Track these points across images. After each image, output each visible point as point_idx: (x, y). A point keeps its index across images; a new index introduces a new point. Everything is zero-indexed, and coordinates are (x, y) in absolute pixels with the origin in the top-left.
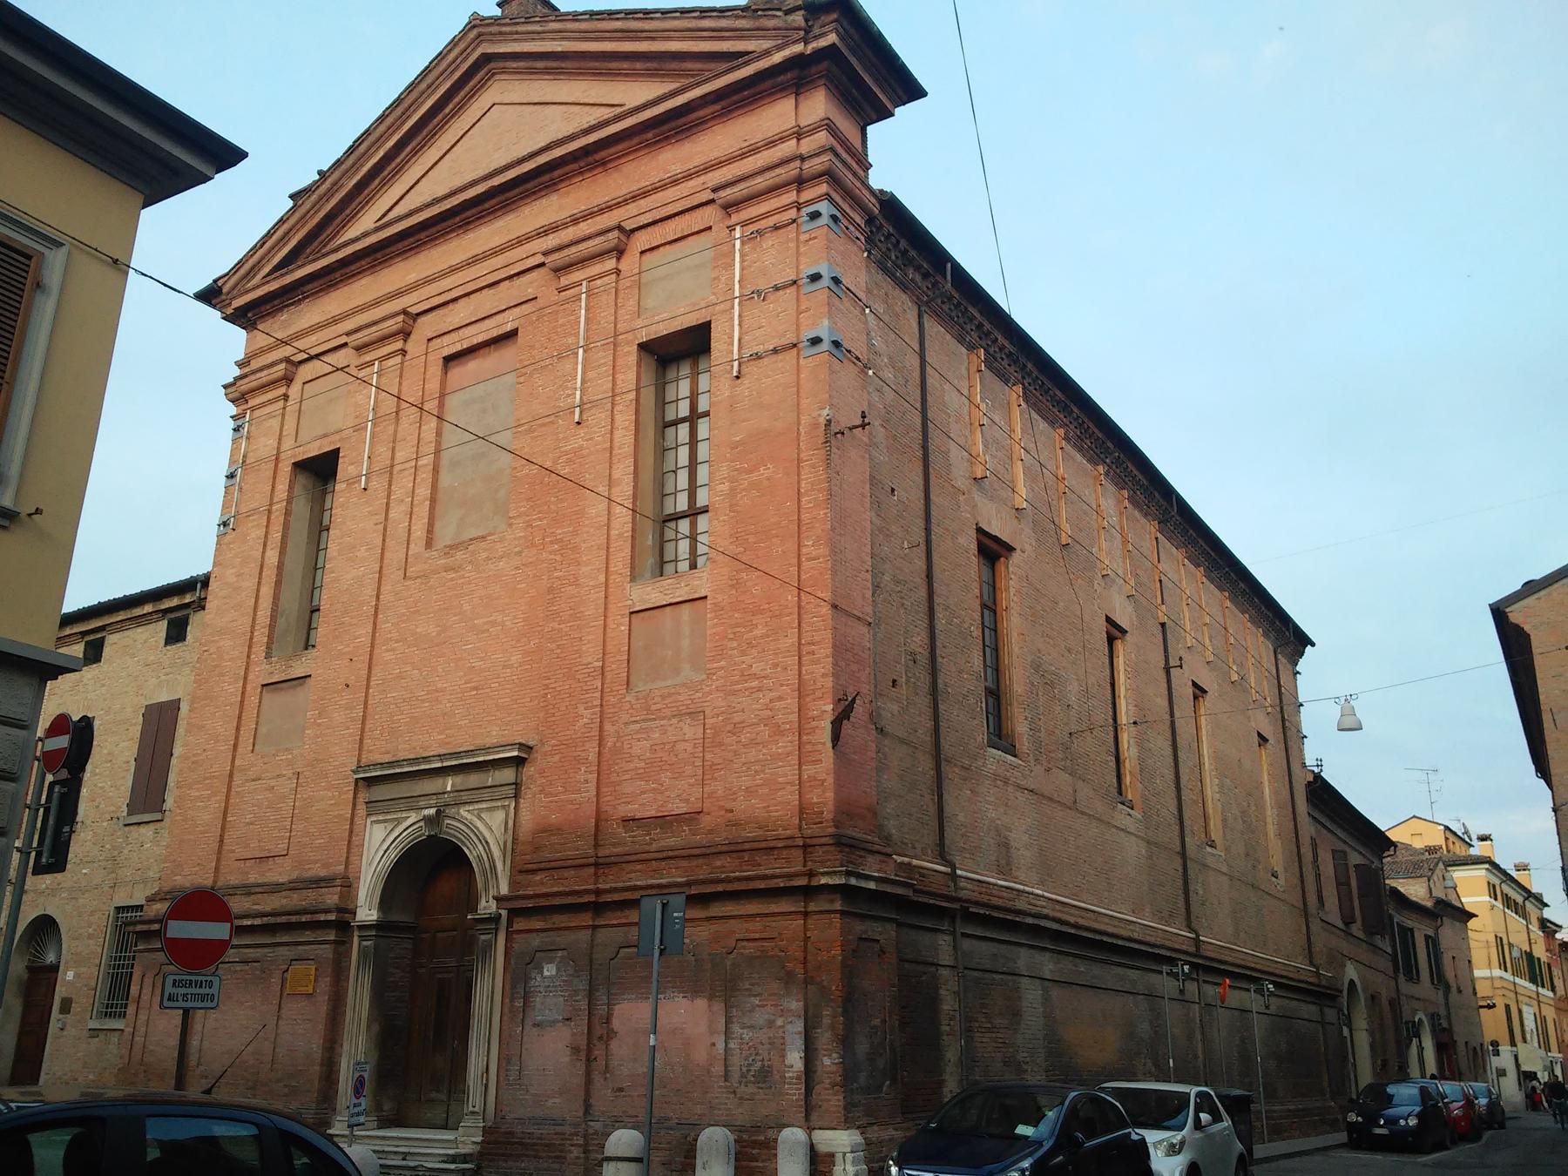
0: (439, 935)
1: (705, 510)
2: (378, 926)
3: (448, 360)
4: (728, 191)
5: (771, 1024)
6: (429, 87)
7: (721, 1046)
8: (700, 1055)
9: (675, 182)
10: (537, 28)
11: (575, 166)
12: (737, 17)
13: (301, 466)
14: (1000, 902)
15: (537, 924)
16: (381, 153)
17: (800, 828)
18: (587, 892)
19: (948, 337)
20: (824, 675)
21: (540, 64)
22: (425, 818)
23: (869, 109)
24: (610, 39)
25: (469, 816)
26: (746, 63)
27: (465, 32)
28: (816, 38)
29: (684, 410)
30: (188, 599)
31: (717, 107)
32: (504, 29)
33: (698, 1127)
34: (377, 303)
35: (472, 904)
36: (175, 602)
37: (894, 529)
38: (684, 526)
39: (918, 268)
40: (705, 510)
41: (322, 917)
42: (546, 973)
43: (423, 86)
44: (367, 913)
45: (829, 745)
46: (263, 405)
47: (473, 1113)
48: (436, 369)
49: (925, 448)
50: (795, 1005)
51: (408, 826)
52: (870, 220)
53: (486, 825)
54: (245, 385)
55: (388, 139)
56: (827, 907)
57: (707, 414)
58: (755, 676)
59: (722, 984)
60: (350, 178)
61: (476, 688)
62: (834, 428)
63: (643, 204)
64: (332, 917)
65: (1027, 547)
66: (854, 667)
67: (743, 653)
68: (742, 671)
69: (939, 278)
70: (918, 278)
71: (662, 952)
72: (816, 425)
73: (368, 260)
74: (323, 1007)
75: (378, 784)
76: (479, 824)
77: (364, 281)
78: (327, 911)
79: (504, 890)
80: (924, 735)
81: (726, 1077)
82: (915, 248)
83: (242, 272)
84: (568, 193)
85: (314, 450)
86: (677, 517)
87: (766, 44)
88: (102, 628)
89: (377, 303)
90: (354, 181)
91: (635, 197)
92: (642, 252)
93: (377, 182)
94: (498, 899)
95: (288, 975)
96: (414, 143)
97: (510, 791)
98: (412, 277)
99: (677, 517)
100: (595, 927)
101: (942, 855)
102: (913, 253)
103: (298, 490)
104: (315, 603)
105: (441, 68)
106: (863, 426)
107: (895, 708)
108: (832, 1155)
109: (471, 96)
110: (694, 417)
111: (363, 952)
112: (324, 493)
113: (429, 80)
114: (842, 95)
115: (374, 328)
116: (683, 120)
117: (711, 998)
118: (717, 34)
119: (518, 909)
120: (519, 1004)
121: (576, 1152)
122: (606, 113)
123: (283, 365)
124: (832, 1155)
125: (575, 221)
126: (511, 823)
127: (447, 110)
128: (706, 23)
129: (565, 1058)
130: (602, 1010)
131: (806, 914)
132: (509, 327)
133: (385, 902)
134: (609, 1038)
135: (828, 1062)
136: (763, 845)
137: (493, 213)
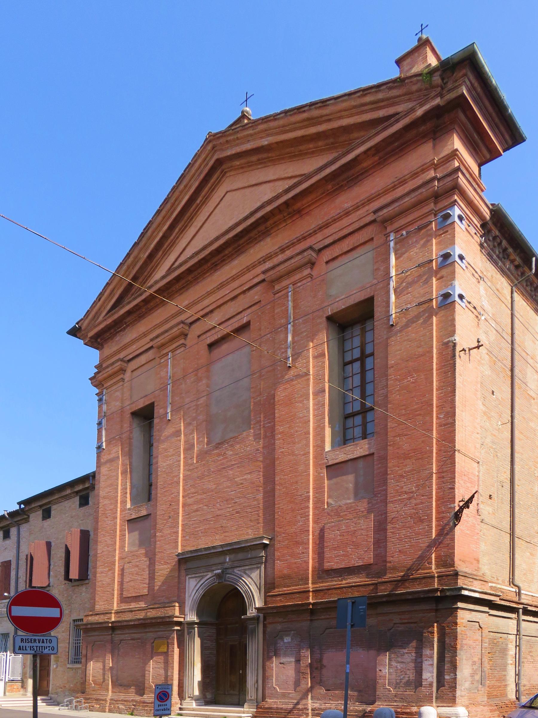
0: (229, 626)
3: (211, 346)
4: (385, 211)
6: (185, 186)
9: (347, 213)
10: (251, 132)
12: (390, 88)
13: (134, 414)
16: (161, 234)
19: (528, 308)
21: (254, 158)
22: (218, 576)
24: (301, 128)
25: (239, 573)
26: (397, 121)
27: (204, 147)
28: (449, 91)
29: (357, 354)
30: (87, 485)
34: (166, 321)
35: (244, 611)
36: (80, 487)
37: (493, 414)
38: (358, 420)
39: (512, 261)
42: (285, 641)
43: (182, 187)
46: (111, 386)
47: (251, 700)
48: (204, 350)
49: (512, 370)
52: (483, 226)
54: (100, 377)
55: (164, 224)
57: (372, 354)
58: (406, 493)
66: (469, 485)
67: (398, 481)
68: (397, 490)
69: (526, 269)
70: (512, 268)
71: (352, 626)
77: (159, 311)
82: (513, 247)
83: (90, 317)
85: (141, 404)
86: (353, 415)
87: (410, 105)
88: (49, 503)
89: (166, 321)
90: (147, 254)
91: (321, 228)
92: (327, 262)
93: (161, 253)
95: (154, 644)
96: (180, 226)
99: (353, 415)
101: (512, 582)
102: (510, 250)
103: (135, 425)
106: (478, 347)
107: (490, 510)
109: (213, 189)
110: (363, 358)
114: (466, 137)
115: (167, 334)
118: (376, 105)
123: (119, 363)
125: (283, 250)
127: (198, 201)
128: (368, 99)
131: (437, 610)
132: (245, 320)
134: (321, 668)
137: (231, 257)
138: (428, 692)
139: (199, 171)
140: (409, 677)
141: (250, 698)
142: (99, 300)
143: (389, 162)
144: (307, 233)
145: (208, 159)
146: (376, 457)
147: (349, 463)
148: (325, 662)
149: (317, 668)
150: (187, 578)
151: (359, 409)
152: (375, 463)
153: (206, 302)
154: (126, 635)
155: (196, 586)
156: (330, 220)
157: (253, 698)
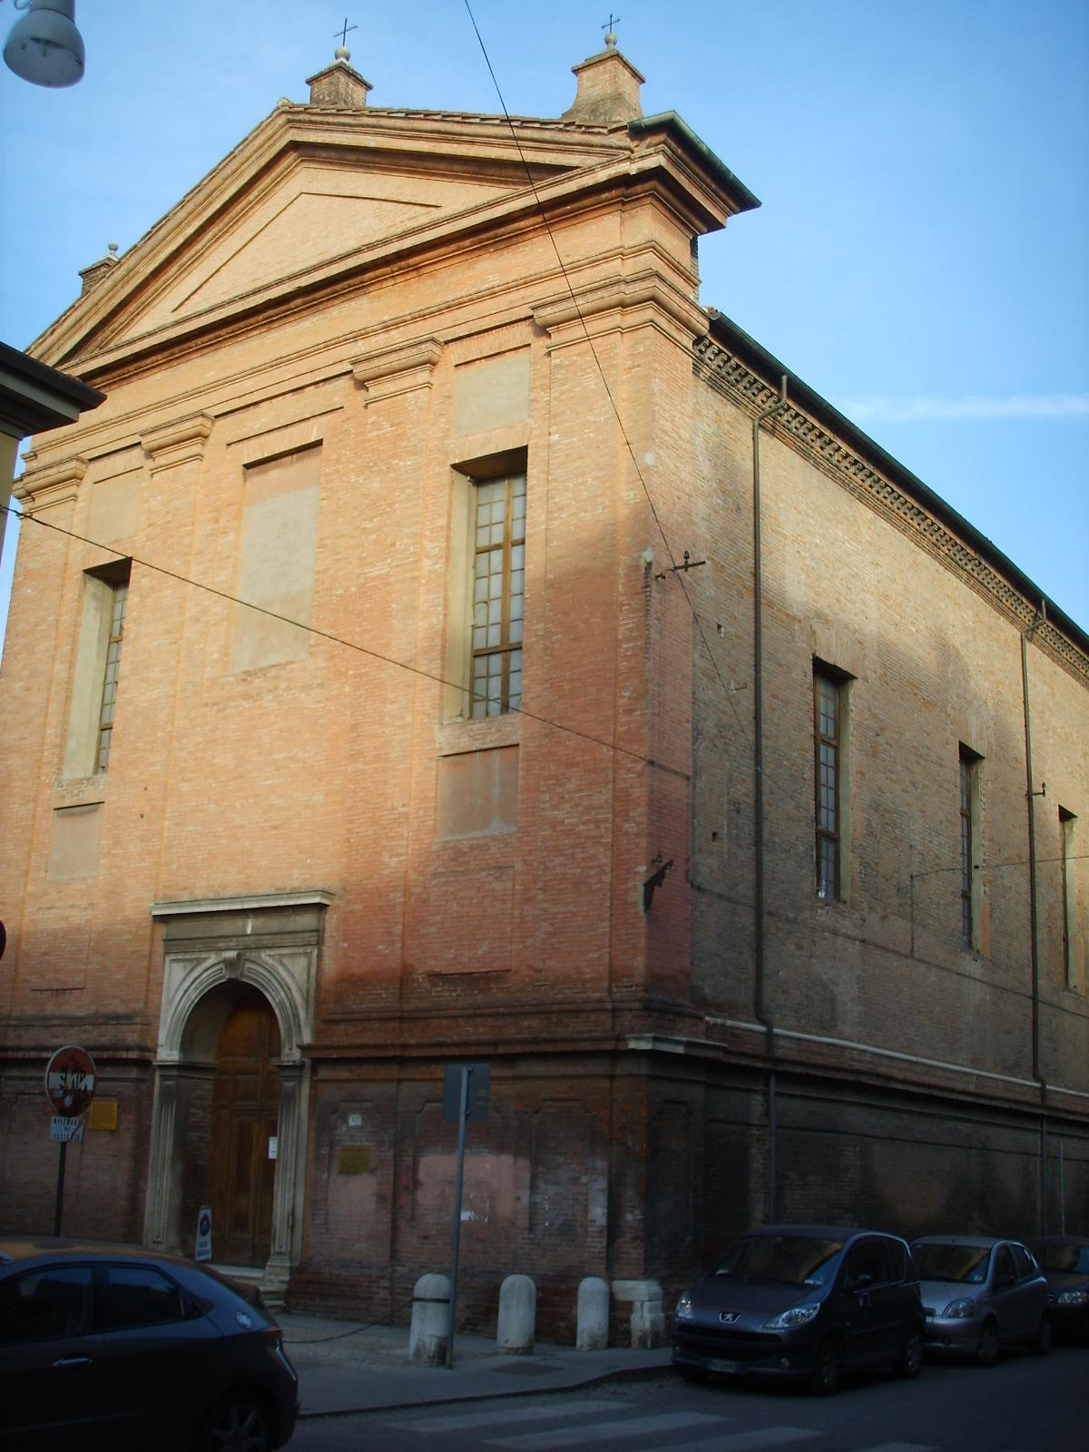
0: (239, 1077)
1: (518, 647)
2: (183, 1067)
5: (575, 1181)
7: (525, 1201)
8: (505, 1207)
9: (492, 294)
11: (388, 269)
14: (821, 1061)
15: (343, 1073)
17: (610, 991)
18: (393, 1046)
20: (637, 835)
22: (229, 964)
23: (698, 223)
25: (270, 961)
31: (539, 219)
32: (314, 118)
33: (501, 1276)
38: (496, 663)
40: (518, 647)
41: (124, 1055)
42: (352, 1123)
43: (228, 171)
44: (168, 1053)
45: (641, 907)
47: (279, 1253)
50: (601, 1164)
51: (208, 969)
52: (699, 339)
53: (288, 970)
55: (189, 224)
56: (635, 1070)
59: (527, 1141)
60: (147, 264)
61: (276, 828)
62: (655, 571)
63: (461, 315)
64: (133, 1055)
65: (870, 674)
67: (556, 807)
72: (636, 568)
73: (165, 354)
74: (128, 1142)
75: (180, 928)
76: (281, 969)
78: (128, 1049)
79: (307, 1038)
80: (746, 889)
81: (531, 1228)
84: (379, 297)
87: (591, 161)
94: (303, 1048)
97: (313, 938)
98: (211, 376)
100: (399, 1081)
104: (106, 720)
105: (246, 153)
108: (630, 1304)
109: (276, 183)
111: (165, 1092)
112: (115, 601)
113: (233, 166)
115: (171, 430)
116: (503, 230)
117: (517, 1154)
119: (318, 1059)
120: (325, 1151)
121: (382, 1294)
122: (424, 217)
123: (74, 464)
124: (630, 1304)
125: (387, 327)
126: (313, 971)
129: (371, 1205)
130: (408, 1160)
131: (612, 1077)
133: (188, 1042)
135: (631, 1217)
136: (573, 1007)
138: (596, 1247)
139: (271, 142)
140: (566, 1215)
141: (277, 1249)
142: (52, 333)
143: (557, 228)
144: (427, 311)
145: (276, 137)
146: (521, 749)
147: (478, 754)
148: (422, 1174)
149: (407, 1188)
150: (167, 959)
151: (497, 643)
152: (520, 765)
153: (248, 385)
154: (31, 1083)
155: (184, 980)
156: (465, 299)
157: (283, 1250)
